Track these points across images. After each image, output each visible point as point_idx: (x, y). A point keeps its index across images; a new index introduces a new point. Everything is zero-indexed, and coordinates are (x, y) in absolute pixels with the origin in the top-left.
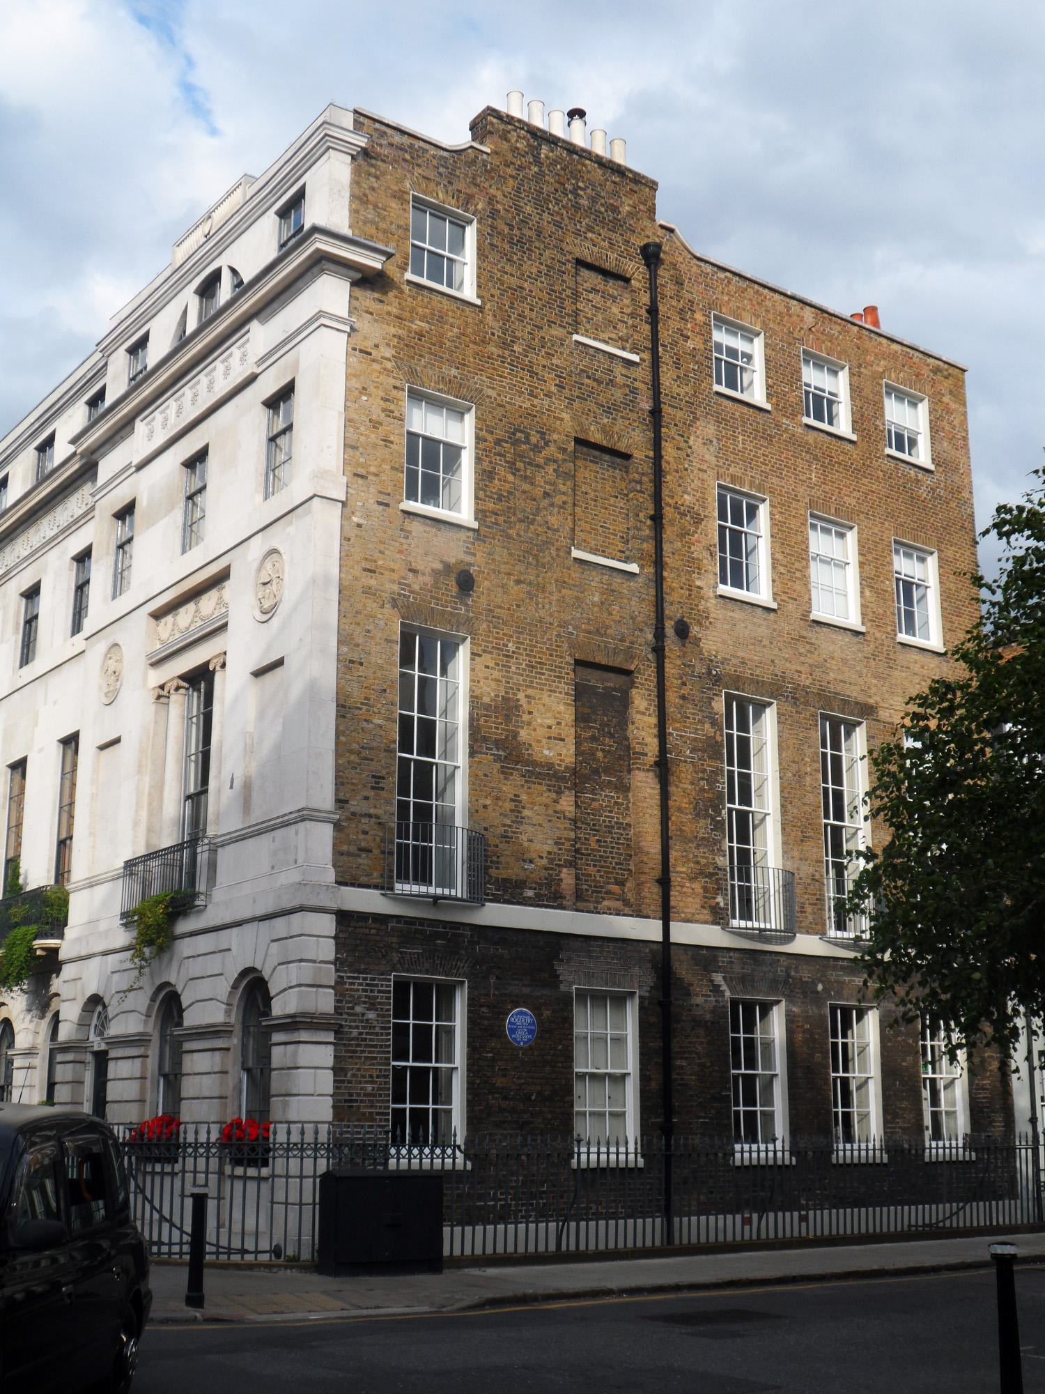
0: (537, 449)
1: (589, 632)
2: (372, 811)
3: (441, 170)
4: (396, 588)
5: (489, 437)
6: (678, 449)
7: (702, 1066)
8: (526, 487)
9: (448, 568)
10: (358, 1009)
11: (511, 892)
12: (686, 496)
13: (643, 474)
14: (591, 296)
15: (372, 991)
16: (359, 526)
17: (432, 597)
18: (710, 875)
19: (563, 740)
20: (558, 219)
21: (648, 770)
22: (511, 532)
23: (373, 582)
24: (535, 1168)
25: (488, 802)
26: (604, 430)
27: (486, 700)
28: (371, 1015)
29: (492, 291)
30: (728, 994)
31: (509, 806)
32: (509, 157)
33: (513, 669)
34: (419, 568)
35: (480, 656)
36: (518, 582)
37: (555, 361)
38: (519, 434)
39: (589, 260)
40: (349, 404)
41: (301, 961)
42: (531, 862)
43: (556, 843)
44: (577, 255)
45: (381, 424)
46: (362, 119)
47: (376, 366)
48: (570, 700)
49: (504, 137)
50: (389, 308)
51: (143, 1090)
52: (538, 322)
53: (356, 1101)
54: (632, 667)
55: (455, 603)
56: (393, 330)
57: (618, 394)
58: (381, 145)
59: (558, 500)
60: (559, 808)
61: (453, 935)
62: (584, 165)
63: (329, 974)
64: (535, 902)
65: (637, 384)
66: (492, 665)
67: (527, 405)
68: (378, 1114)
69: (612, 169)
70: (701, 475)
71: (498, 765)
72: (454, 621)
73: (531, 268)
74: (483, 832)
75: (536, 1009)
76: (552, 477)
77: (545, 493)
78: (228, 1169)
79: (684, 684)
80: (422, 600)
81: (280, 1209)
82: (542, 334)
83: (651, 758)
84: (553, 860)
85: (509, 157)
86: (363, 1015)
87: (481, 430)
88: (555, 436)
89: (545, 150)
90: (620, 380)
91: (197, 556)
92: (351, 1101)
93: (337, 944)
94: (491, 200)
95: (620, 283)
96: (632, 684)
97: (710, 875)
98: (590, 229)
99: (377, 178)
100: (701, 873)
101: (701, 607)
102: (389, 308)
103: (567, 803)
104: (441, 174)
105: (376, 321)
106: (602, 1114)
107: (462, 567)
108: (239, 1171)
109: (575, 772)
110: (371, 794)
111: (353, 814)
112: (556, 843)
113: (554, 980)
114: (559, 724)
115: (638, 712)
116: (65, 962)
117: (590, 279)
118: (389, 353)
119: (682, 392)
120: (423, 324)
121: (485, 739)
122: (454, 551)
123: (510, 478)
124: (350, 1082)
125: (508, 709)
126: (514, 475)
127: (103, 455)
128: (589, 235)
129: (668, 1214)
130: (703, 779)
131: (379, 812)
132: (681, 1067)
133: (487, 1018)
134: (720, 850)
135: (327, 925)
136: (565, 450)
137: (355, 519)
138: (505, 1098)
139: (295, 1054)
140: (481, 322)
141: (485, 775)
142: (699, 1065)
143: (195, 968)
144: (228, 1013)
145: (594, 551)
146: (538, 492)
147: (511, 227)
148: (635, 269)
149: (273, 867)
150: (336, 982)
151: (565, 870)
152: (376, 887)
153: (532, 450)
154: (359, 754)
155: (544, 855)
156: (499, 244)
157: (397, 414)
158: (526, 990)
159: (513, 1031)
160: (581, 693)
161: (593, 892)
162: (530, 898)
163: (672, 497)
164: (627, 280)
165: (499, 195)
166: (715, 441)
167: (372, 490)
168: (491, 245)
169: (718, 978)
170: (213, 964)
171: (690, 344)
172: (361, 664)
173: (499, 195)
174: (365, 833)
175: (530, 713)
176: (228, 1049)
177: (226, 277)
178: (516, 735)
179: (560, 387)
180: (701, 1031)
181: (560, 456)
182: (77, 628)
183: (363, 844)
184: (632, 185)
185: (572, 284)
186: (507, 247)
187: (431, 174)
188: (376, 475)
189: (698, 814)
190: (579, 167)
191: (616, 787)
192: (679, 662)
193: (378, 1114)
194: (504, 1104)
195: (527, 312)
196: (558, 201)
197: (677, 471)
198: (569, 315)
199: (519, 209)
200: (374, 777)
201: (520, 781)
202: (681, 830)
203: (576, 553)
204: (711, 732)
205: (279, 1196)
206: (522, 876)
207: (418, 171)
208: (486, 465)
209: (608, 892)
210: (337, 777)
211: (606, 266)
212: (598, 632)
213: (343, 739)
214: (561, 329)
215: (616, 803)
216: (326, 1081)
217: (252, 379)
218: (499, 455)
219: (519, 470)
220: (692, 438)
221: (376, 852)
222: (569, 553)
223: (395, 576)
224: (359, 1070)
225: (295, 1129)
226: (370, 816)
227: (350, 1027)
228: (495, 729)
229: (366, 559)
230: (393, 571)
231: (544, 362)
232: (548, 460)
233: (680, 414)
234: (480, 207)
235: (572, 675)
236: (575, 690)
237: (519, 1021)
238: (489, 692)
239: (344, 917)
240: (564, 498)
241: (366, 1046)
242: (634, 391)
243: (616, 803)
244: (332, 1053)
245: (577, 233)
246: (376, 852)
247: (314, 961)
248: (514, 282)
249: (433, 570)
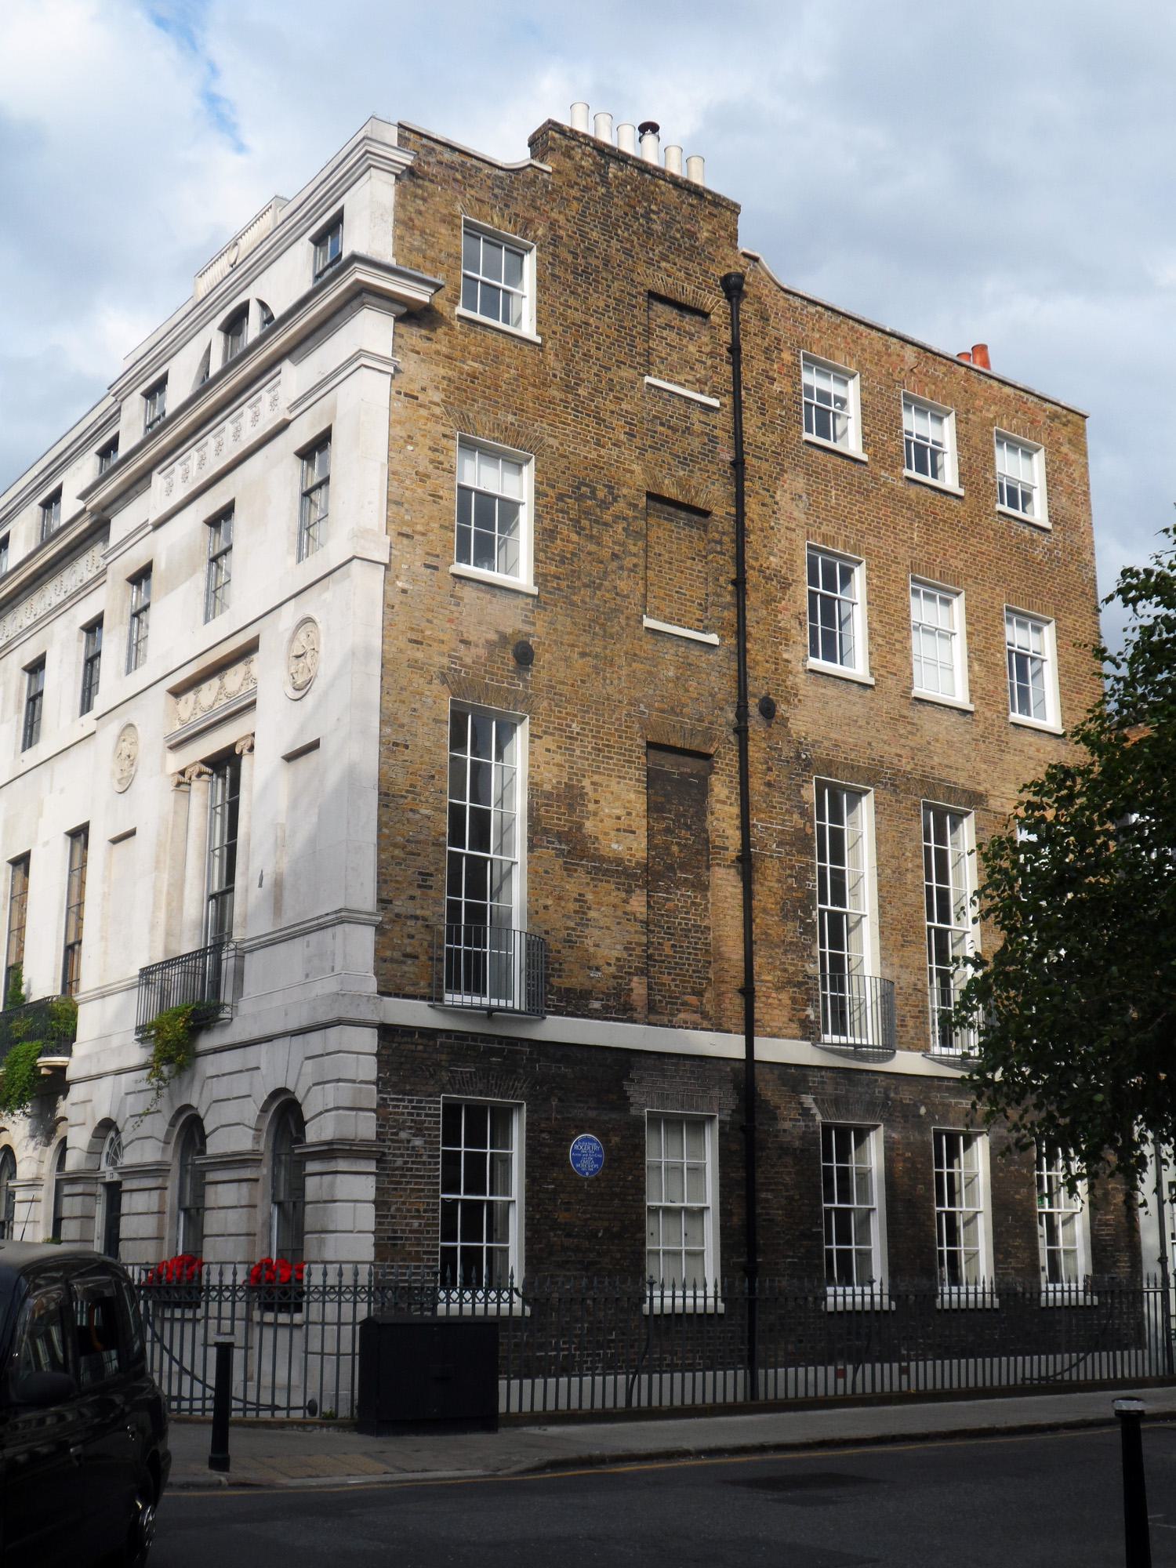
0: (604, 505)
1: (663, 711)
2: (419, 912)
3: (496, 191)
4: (445, 661)
5: (550, 492)
6: (763, 505)
7: (790, 1199)
8: (592, 547)
9: (504, 639)
10: (403, 1135)
11: (575, 1004)
12: (772, 558)
13: (724, 533)
14: (665, 333)
15: (418, 1115)
16: (404, 591)
17: (486, 671)
18: (799, 985)
19: (634, 832)
20: (628, 246)
21: (729, 867)
22: (575, 598)
23: (419, 655)
24: (602, 1314)
25: (549, 902)
26: (679, 484)
27: (547, 787)
28: (418, 1142)
29: (554, 327)
30: (819, 1118)
31: (572, 906)
32: (573, 177)
33: (578, 752)
34: (471, 638)
35: (540, 737)
36: (583, 655)
37: (624, 406)
38: (584, 489)
39: (663, 293)
40: (393, 454)
41: (339, 1080)
42: (598, 969)
43: (626, 948)
44: (650, 287)
45: (428, 477)
46: (407, 134)
47: (423, 412)
48: (642, 787)
49: (568, 154)
50: (438, 347)
51: (160, 1226)
52: (606, 362)
53: (401, 1238)
54: (712, 751)
55: (512, 678)
56: (442, 372)
57: (696, 444)
58: (429, 164)
59: (628, 562)
60: (629, 908)
61: (510, 1051)
62: (657, 186)
63: (371, 1096)
64: (602, 1015)
65: (717, 432)
66: (553, 748)
67: (593, 455)
68: (425, 1253)
69: (689, 190)
70: (789, 534)
71: (561, 861)
72: (511, 698)
73: (598, 301)
74: (543, 936)
75: (603, 1135)
76: (621, 536)
77: (613, 554)
78: (256, 1315)
79: (770, 769)
80: (475, 675)
81: (315, 1360)
82: (610, 375)
83: (733, 852)
84: (622, 967)
85: (573, 177)
86: (409, 1141)
87: (541, 483)
88: (625, 491)
89: (613, 169)
90: (697, 427)
91: (222, 626)
92: (395, 1238)
93: (379, 1062)
94: (553, 225)
95: (698, 318)
96: (712, 770)
97: (799, 985)
98: (664, 257)
99: (424, 200)
100: (789, 982)
101: (789, 683)
102: (438, 347)
103: (638, 904)
104: (496, 196)
105: (423, 361)
106: (678, 1254)
107: (520, 638)
108: (269, 1317)
109: (647, 868)
110: (418, 893)
111: (398, 915)
112: (626, 948)
113: (624, 1102)
114: (629, 814)
115: (718, 801)
116: (74, 1082)
117: (664, 314)
118: (437, 397)
119: (768, 441)
120: (476, 365)
121: (546, 831)
122: (511, 619)
123: (574, 537)
124: (393, 1217)
125: (571, 797)
126: (579, 534)
127: (116, 512)
128: (663, 264)
129: (751, 1365)
130: (791, 876)
131: (427, 913)
132: (767, 1200)
133: (548, 1146)
134: (810, 956)
135: (368, 1040)
136: (635, 506)
137: (400, 584)
138: (569, 1235)
139: (332, 1185)
140: (541, 362)
141: (546, 872)
142: (787, 1198)
143: (220, 1088)
144: (256, 1139)
145: (668, 620)
146: (606, 553)
147: (575, 255)
148: (715, 302)
149: (307, 976)
150: (379, 1105)
151: (635, 979)
152: (423, 998)
153: (599, 506)
154: (404, 848)
155: (613, 962)
156: (562, 274)
157: (446, 466)
158: (592, 1114)
159: (577, 1160)
160: (653, 779)
161: (668, 1003)
162: (596, 1010)
163: (757, 559)
164: (706, 315)
165: (561, 219)
166: (804, 496)
167: (419, 551)
168: (553, 275)
169: (808, 1100)
170: (240, 1084)
171: (777, 387)
172: (407, 747)
173: (561, 219)
174: (411, 937)
175: (597, 802)
176: (256, 1180)
177: (254, 311)
178: (580, 826)
179: (631, 435)
180: (789, 1160)
181: (631, 513)
182: (86, 706)
183: (409, 950)
184: (711, 209)
185: (644, 320)
186: (570, 277)
187: (485, 195)
188: (423, 534)
189: (786, 915)
190: (652, 188)
191: (693, 886)
192: (764, 745)
193: (425, 1253)
194: (568, 1242)
195: (593, 351)
196: (628, 226)
197: (762, 530)
198: (640, 355)
199: (584, 235)
200: (420, 873)
201: (585, 878)
202: (766, 933)
203: (648, 622)
204: (800, 823)
205: (315, 1345)
206: (588, 985)
207: (470, 192)
208: (547, 523)
209: (684, 1004)
210: (379, 874)
211: (682, 299)
212: (673, 711)
213: (386, 831)
214: (631, 371)
215: (693, 903)
216: (367, 1216)
217: (284, 426)
218: (562, 511)
219: (584, 529)
220: (779, 493)
221: (423, 958)
222: (641, 622)
223: (445, 648)
224: (404, 1203)
225: (332, 1269)
226: (416, 918)
227: (394, 1155)
228: (557, 820)
229: (412, 629)
230: (443, 642)
231: (612, 407)
232: (617, 518)
233: (765, 465)
234: (540, 232)
235: (644, 760)
236: (648, 776)
237: (584, 1148)
238: (550, 779)
239: (387, 1032)
240: (635, 560)
241: (412, 1176)
242: (713, 440)
243: (693, 903)
244: (374, 1184)
245: (650, 262)
246: (423, 958)
247: (354, 1081)
248: (578, 317)
249: (487, 641)
